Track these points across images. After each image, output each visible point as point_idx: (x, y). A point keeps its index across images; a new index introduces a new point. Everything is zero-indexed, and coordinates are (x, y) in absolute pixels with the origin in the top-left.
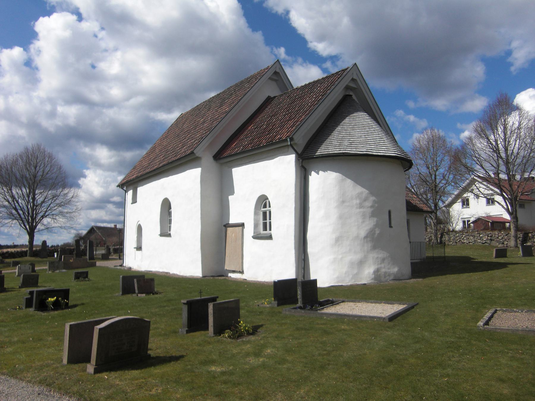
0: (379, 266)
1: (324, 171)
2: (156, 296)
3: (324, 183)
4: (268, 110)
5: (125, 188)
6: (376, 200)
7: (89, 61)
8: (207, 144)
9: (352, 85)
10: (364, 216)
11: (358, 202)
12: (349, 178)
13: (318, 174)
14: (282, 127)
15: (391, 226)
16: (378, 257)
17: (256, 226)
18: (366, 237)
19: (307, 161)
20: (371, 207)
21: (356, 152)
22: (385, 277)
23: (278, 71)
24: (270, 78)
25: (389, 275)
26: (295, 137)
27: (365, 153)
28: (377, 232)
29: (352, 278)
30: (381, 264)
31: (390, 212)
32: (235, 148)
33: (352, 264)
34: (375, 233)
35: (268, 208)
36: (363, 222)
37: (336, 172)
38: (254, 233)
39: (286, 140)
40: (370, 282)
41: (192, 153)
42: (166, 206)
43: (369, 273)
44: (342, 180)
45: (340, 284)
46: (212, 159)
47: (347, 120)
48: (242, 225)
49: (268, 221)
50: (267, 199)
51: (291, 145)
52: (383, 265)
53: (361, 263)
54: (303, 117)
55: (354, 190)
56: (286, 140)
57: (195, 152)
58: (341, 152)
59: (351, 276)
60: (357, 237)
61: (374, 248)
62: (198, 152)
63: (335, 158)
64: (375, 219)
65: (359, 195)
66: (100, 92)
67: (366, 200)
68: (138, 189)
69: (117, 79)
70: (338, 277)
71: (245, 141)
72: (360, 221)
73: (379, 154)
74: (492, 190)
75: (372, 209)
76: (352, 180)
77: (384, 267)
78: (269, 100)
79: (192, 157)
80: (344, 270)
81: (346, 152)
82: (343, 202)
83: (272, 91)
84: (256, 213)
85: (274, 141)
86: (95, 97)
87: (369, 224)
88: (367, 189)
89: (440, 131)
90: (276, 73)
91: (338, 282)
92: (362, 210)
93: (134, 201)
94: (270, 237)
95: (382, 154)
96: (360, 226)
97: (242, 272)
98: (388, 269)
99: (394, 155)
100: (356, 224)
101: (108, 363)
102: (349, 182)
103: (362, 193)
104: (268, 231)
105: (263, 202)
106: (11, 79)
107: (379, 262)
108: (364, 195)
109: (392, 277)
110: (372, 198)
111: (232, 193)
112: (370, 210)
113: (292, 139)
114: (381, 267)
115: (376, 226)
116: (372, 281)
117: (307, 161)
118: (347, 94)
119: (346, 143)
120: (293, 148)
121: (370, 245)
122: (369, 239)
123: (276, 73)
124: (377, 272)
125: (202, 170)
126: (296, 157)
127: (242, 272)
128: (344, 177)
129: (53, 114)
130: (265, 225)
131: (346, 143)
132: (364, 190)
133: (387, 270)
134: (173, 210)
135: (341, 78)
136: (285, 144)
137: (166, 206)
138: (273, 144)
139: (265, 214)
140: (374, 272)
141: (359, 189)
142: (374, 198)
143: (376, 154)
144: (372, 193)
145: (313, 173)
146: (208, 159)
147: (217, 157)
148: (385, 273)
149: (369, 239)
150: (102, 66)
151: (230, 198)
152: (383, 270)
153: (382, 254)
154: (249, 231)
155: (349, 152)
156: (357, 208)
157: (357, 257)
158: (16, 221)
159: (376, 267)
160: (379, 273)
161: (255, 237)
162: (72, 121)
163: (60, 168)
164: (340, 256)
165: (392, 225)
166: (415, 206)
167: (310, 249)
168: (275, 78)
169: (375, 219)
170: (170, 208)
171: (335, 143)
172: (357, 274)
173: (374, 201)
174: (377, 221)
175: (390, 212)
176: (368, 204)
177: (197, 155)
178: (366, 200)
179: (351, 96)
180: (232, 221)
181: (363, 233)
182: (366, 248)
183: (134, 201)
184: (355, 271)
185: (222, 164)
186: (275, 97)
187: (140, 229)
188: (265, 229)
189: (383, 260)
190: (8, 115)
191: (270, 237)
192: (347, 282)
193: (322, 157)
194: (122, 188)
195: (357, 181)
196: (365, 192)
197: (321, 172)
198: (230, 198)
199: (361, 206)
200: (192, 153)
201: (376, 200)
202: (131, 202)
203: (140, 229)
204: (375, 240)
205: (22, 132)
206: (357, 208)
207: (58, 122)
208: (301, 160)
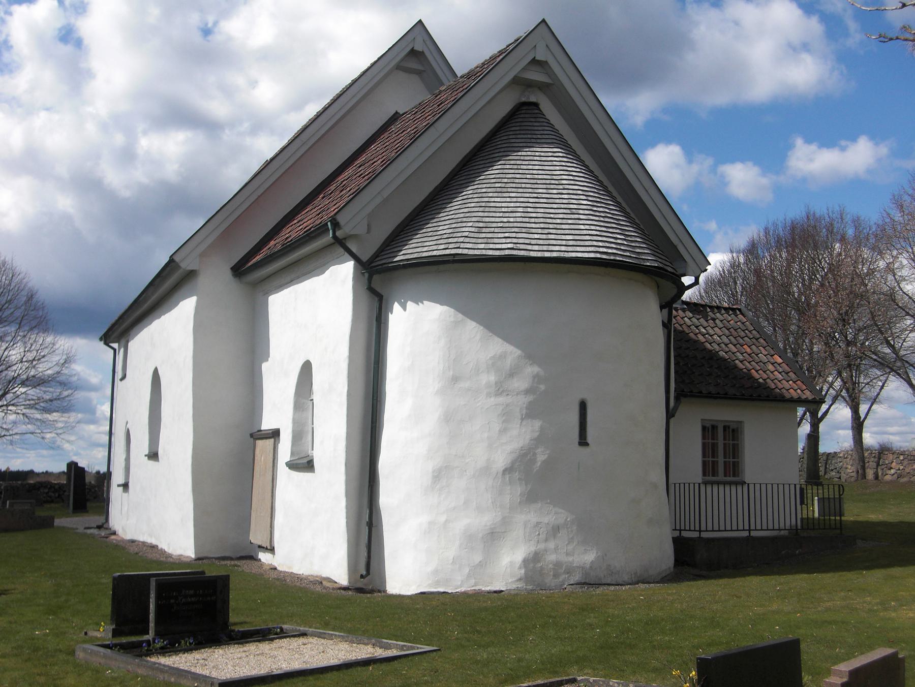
0: (542, 546)
1: (417, 301)
6: (542, 373)
7: (195, 19)
8: (210, 241)
9: (536, 76)
10: (506, 416)
11: (492, 378)
12: (472, 319)
13: (405, 309)
15: (583, 441)
16: (538, 523)
18: (508, 470)
19: (381, 280)
20: (527, 392)
21: (484, 252)
22: (556, 576)
23: (418, 48)
25: (569, 571)
27: (507, 252)
28: (541, 457)
29: (469, 576)
30: (546, 540)
31: (583, 406)
33: (469, 538)
34: (533, 461)
36: (503, 431)
37: (441, 304)
38: (292, 454)
40: (514, 586)
43: (512, 563)
44: (456, 324)
45: (441, 590)
46: (229, 273)
47: (494, 171)
52: (551, 545)
53: (493, 537)
55: (482, 347)
58: (447, 252)
59: (467, 570)
60: (486, 470)
61: (530, 498)
63: (441, 267)
64: (537, 424)
65: (495, 363)
66: (228, 92)
67: (512, 374)
69: (269, 57)
70: (436, 572)
72: (496, 427)
73: (547, 255)
75: (530, 398)
76: (479, 322)
77: (556, 549)
80: (451, 553)
81: (459, 251)
82: (455, 379)
86: (218, 108)
87: (520, 436)
88: (518, 347)
91: (438, 583)
92: (501, 399)
95: (555, 255)
96: (497, 441)
98: (567, 554)
99: (592, 255)
100: (486, 435)
102: (472, 328)
103: (503, 356)
106: (32, 76)
107: (543, 536)
108: (509, 362)
109: (576, 578)
110: (532, 370)
112: (523, 401)
113: (336, 225)
114: (546, 550)
115: (538, 441)
116: (520, 585)
117: (381, 280)
118: (523, 99)
120: (342, 246)
121: (519, 489)
122: (516, 475)
123: (413, 53)
124: (532, 561)
125: (198, 302)
126: (355, 268)
128: (460, 315)
129: (127, 156)
132: (510, 348)
133: (564, 558)
140: (526, 562)
141: (497, 346)
142: (536, 369)
143: (539, 254)
144: (530, 357)
145: (396, 307)
147: (239, 270)
148: (558, 564)
149: (516, 475)
150: (233, 27)
152: (552, 557)
153: (551, 516)
155: (465, 252)
156: (489, 395)
157: (486, 520)
159: (533, 549)
160: (539, 565)
162: (171, 171)
163: (31, 297)
164: (443, 519)
165: (590, 439)
166: (764, 387)
167: (387, 498)
168: (413, 64)
169: (537, 424)
172: (480, 565)
173: (536, 377)
174: (542, 429)
175: (583, 406)
176: (520, 384)
178: (512, 374)
179: (536, 105)
181: (501, 460)
182: (507, 499)
184: (477, 558)
189: (555, 531)
190: (30, 163)
192: (458, 584)
193: (405, 267)
195: (493, 325)
196: (513, 352)
197: (410, 305)
199: (500, 390)
201: (542, 373)
204: (531, 477)
205: (66, 203)
206: (489, 395)
207: (140, 175)
208: (367, 275)
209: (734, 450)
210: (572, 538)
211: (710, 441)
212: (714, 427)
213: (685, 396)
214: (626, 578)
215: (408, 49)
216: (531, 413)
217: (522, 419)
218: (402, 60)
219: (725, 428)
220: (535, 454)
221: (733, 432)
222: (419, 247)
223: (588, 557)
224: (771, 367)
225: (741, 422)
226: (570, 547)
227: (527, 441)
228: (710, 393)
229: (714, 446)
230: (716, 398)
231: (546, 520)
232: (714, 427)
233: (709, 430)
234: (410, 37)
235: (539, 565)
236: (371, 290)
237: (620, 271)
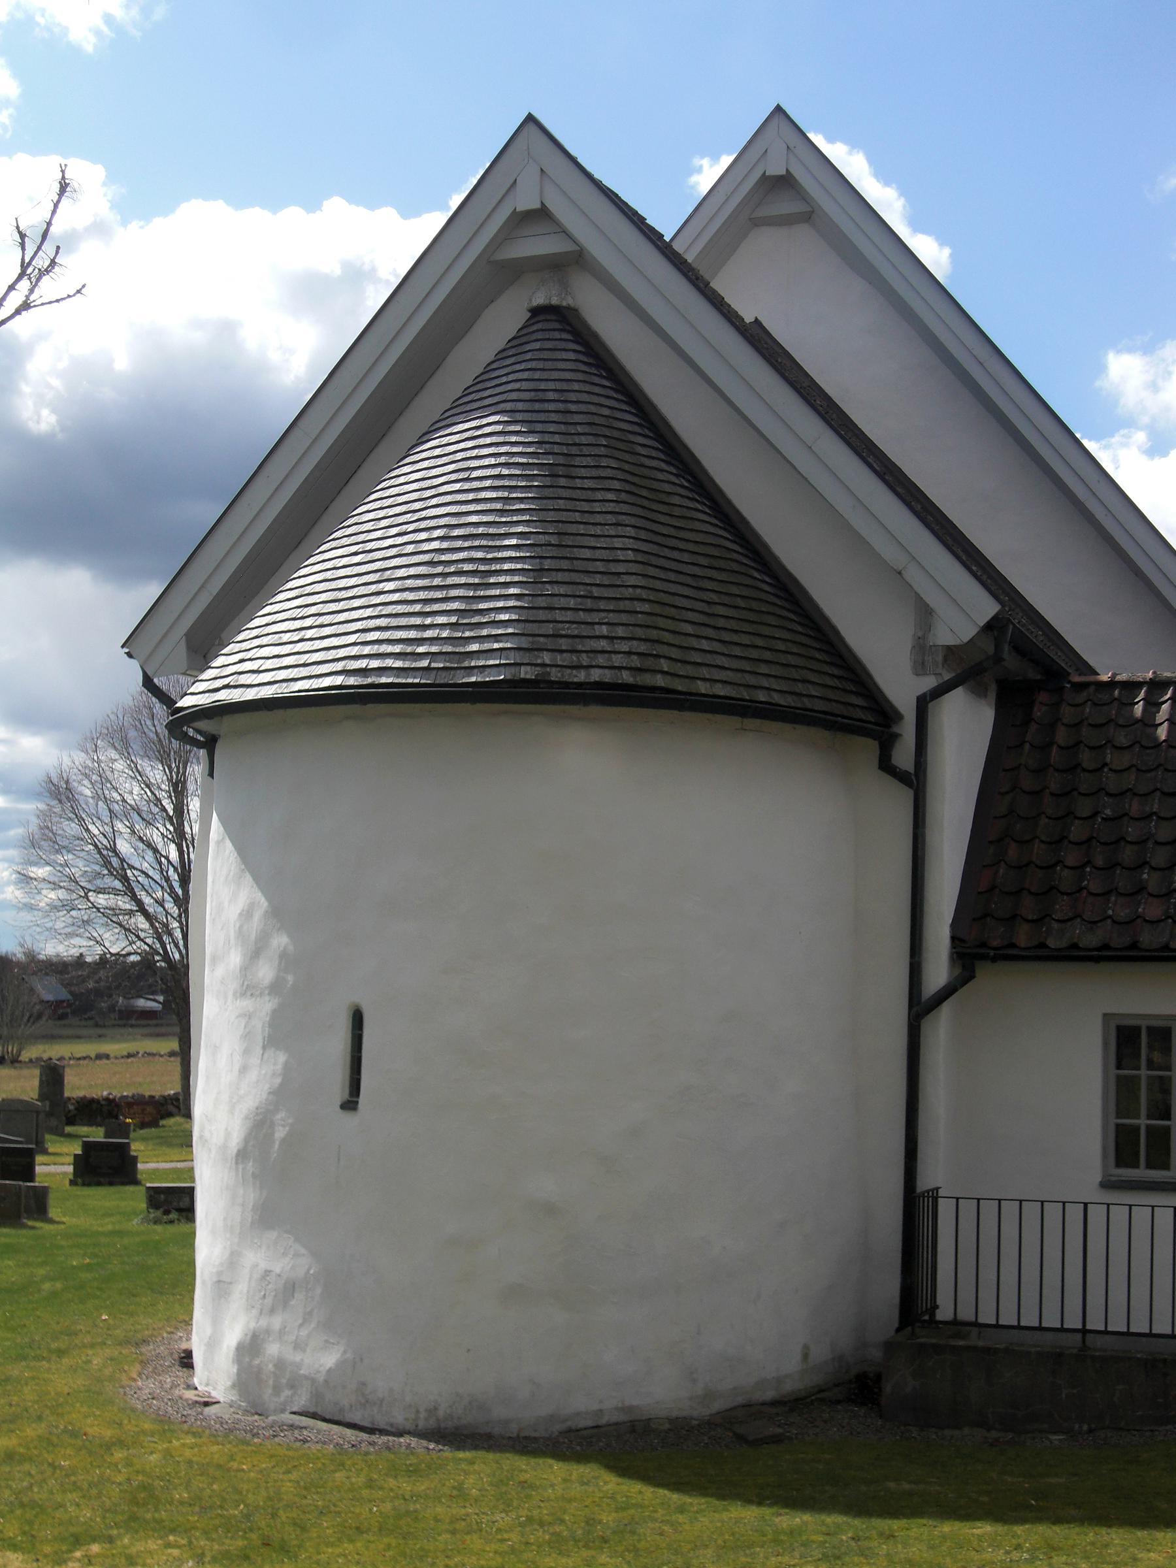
0: (263, 1323)
2: (51, 1227)
16: (267, 1272)
22: (277, 1390)
30: (272, 1311)
31: (358, 1019)
52: (276, 1322)
64: (282, 1058)
77: (282, 1332)
89: (1044, 708)
99: (338, 680)
101: (1167, 1050)
109: (302, 1400)
114: (268, 1332)
123: (784, 183)
148: (280, 1364)
158: (112, 951)
159: (252, 1325)
160: (257, 1362)
168: (785, 206)
174: (286, 1066)
175: (358, 1019)
189: (288, 1290)
210: (310, 1313)
211: (1144, 1072)
213: (1008, 954)
214: (399, 1418)
215: (756, 176)
217: (264, 1048)
218: (498, 241)
220: (272, 1125)
223: (323, 1359)
226: (304, 1333)
227: (265, 1096)
228: (1075, 946)
230: (1097, 960)
233: (1129, 1042)
234: (755, 153)
235: (257, 1362)
237: (236, 716)
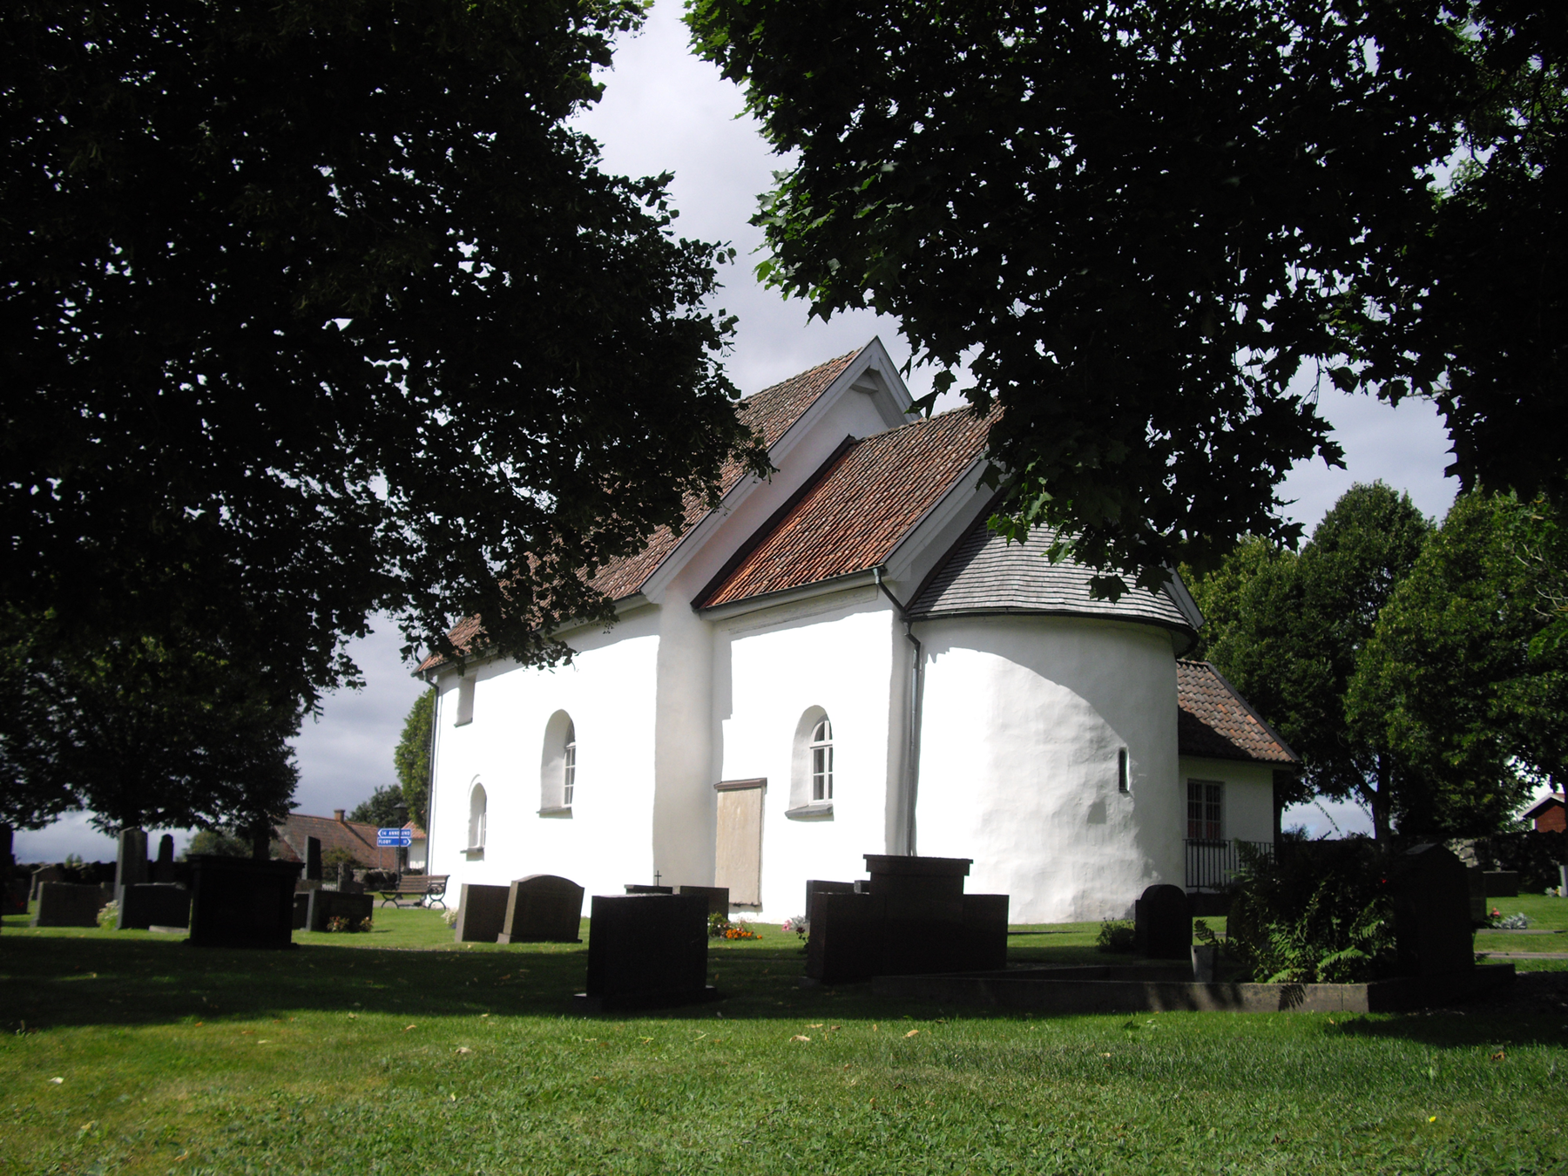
0: (1089, 885)
3: (965, 676)
4: (840, 478)
5: (435, 680)
11: (1041, 726)
14: (866, 534)
17: (796, 785)
18: (1057, 814)
20: (1075, 739)
23: (875, 367)
24: (854, 388)
26: (890, 567)
32: (744, 582)
35: (826, 741)
39: (869, 572)
41: (639, 593)
42: (562, 732)
46: (689, 608)
48: (762, 784)
49: (826, 774)
50: (825, 717)
51: (882, 586)
52: (1097, 884)
54: (918, 512)
56: (869, 572)
57: (644, 591)
62: (652, 593)
67: (1060, 722)
68: (478, 685)
71: (773, 564)
74: (352, 830)
75: (1076, 746)
78: (848, 446)
79: (636, 603)
82: (1005, 727)
83: (862, 422)
84: (797, 754)
85: (843, 573)
90: (870, 373)
92: (1050, 747)
93: (465, 718)
94: (827, 814)
97: (757, 907)
104: (825, 801)
105: (816, 723)
111: (727, 714)
112: (1070, 748)
113: (883, 571)
117: (919, 622)
119: (1016, 582)
123: (870, 373)
127: (757, 907)
130: (819, 783)
131: (1016, 582)
134: (579, 743)
135: (964, 472)
136: (867, 581)
137: (562, 732)
138: (840, 580)
139: (819, 754)
140: (1075, 899)
146: (676, 608)
147: (701, 604)
148: (1103, 901)
151: (725, 722)
152: (1099, 896)
154: (778, 800)
159: (1081, 887)
160: (1086, 902)
161: (792, 815)
170: (571, 737)
171: (990, 580)
176: (1068, 732)
177: (650, 599)
178: (1060, 722)
180: (728, 775)
181: (1051, 804)
183: (465, 718)
185: (714, 624)
186: (862, 441)
187: (479, 798)
188: (819, 793)
189: (1100, 870)
191: (827, 814)
194: (428, 681)
198: (725, 722)
199: (1048, 737)
200: (639, 593)
202: (455, 719)
203: (479, 798)
209: (1215, 812)
212: (1198, 787)
216: (1077, 760)
219: (1208, 788)
221: (1215, 791)
222: (949, 600)
224: (1247, 727)
225: (1222, 783)
229: (1199, 806)
231: (1092, 860)
232: (1198, 787)
236: (911, 638)
